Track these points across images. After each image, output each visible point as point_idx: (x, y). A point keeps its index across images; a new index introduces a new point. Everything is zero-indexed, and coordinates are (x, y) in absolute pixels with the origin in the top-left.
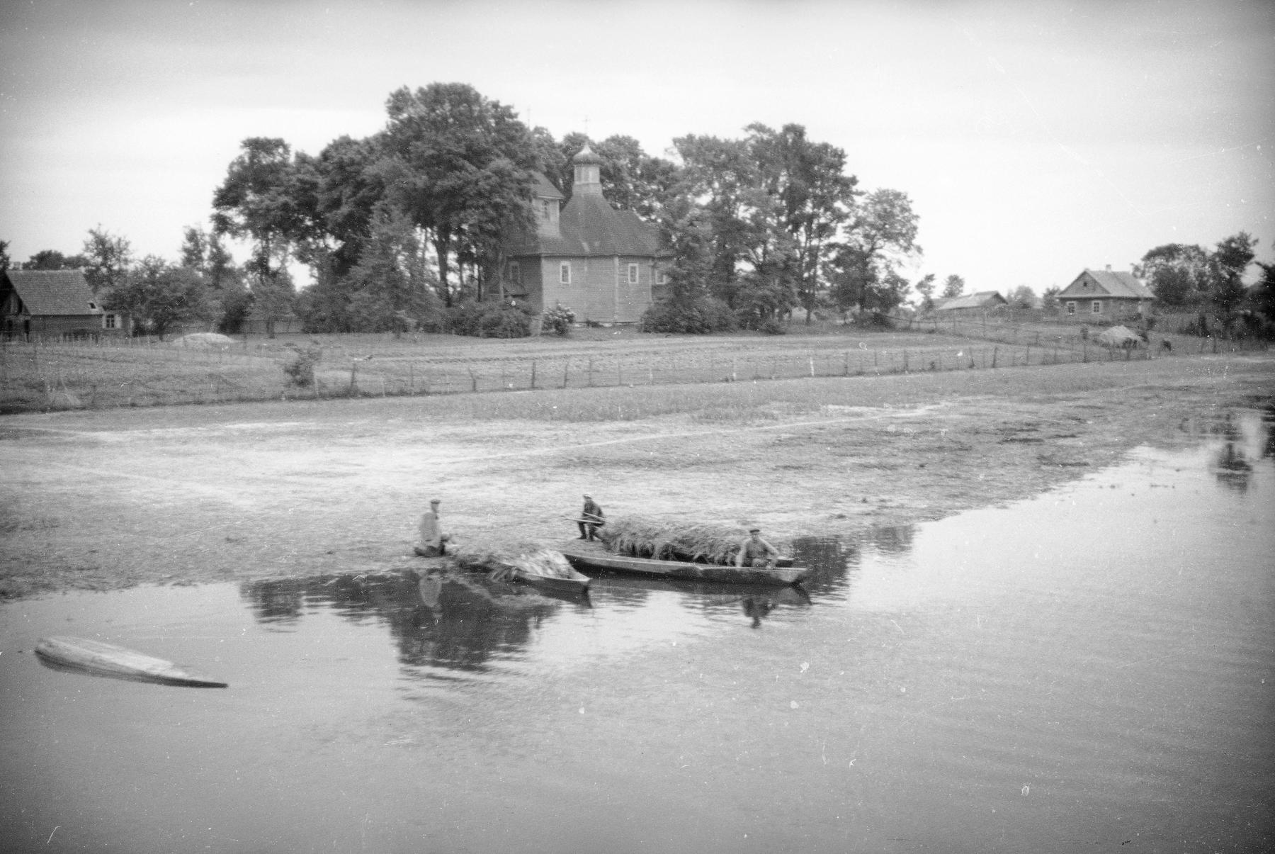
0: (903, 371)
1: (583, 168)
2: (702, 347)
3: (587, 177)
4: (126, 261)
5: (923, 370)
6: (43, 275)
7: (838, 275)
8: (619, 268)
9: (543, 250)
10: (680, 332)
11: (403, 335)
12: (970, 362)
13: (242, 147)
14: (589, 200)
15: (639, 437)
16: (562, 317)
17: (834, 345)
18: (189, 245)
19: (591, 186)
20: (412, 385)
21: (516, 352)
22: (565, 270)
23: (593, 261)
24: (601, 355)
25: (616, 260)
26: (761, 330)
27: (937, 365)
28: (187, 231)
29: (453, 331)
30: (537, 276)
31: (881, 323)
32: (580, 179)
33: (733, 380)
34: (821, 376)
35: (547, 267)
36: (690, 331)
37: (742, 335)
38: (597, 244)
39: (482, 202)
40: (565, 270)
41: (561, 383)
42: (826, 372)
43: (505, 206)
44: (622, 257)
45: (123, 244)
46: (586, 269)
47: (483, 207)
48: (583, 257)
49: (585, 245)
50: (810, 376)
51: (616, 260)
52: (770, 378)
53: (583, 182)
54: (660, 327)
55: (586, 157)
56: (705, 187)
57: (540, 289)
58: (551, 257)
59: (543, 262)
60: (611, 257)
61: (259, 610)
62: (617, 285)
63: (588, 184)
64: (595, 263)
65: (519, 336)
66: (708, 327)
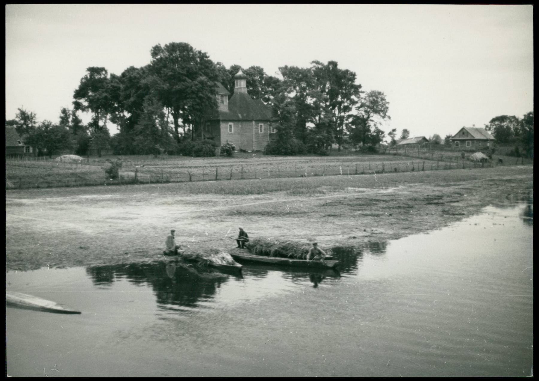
1: (239, 81)
3: (240, 85)
4: (35, 123)
9: (221, 118)
12: (412, 168)
13: (87, 71)
14: (242, 95)
19: (243, 89)
25: (254, 122)
27: (398, 170)
28: (62, 109)
32: (237, 85)
35: (223, 125)
37: (310, 156)
38: (245, 115)
40: (231, 126)
41: (229, 177)
43: (204, 98)
45: (33, 115)
46: (240, 126)
49: (240, 115)
50: (340, 174)
51: (254, 122)
53: (239, 87)
54: (273, 152)
59: (221, 123)
60: (252, 121)
64: (245, 124)
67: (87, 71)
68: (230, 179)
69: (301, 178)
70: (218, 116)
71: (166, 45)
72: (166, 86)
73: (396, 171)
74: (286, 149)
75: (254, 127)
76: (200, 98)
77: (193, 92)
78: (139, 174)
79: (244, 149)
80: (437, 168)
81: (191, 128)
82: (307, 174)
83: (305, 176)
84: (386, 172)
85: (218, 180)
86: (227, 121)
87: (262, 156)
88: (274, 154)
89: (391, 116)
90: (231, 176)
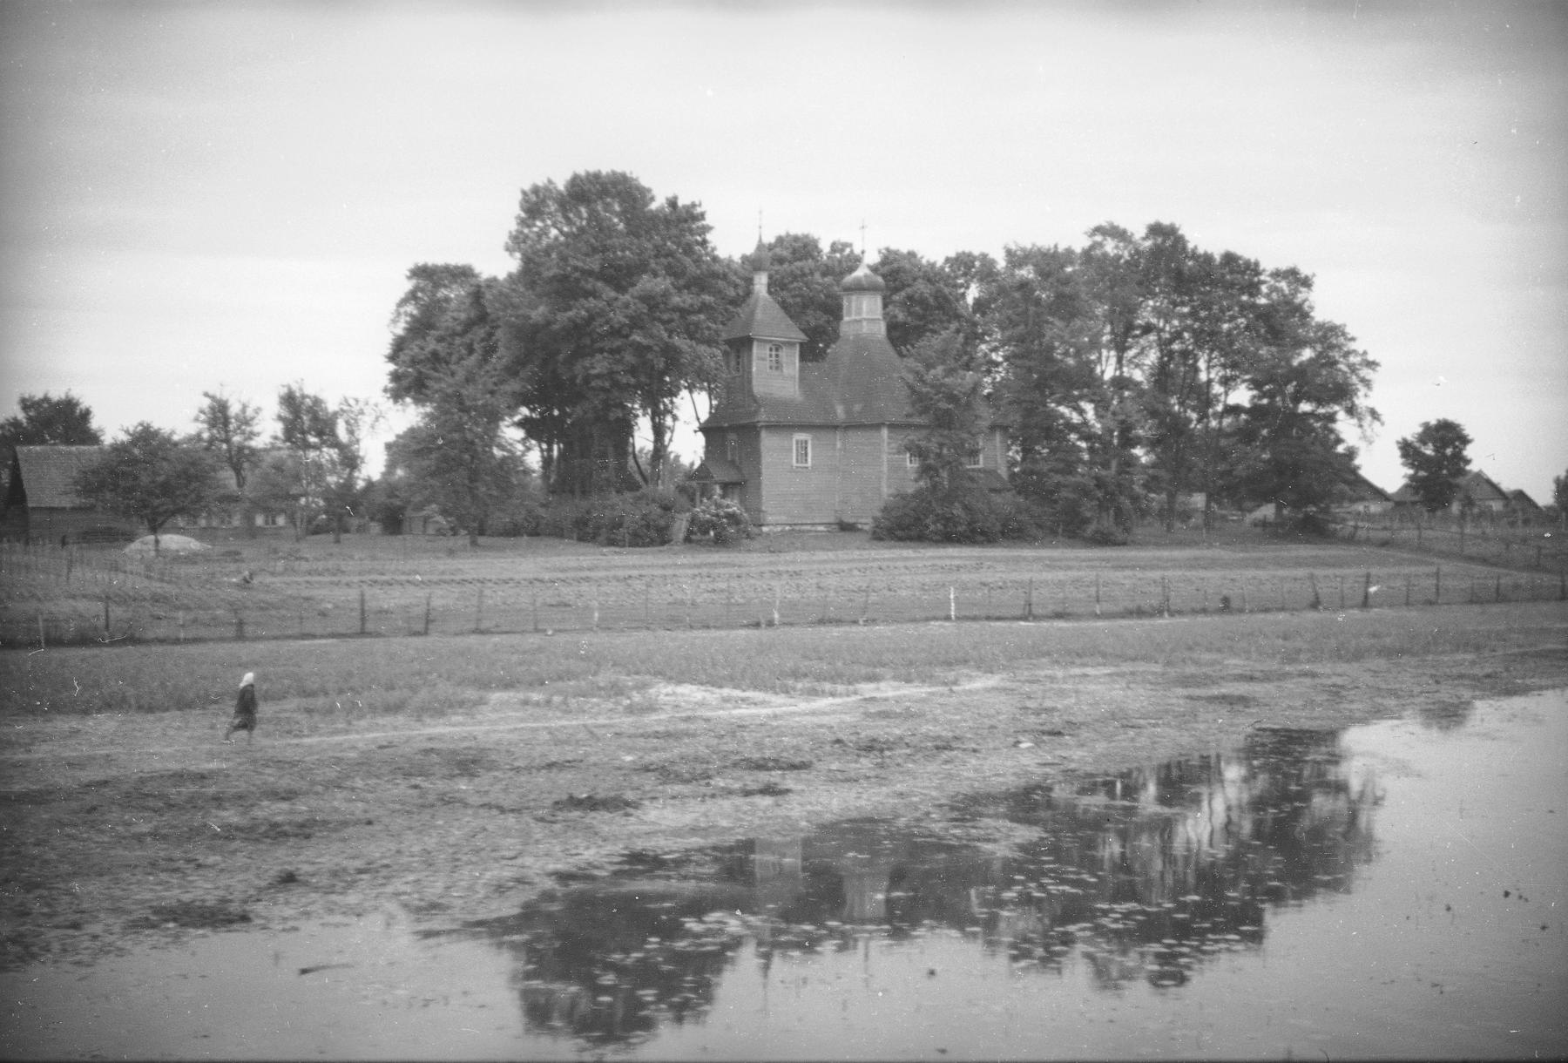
0: (1158, 612)
1: (854, 298)
2: (884, 564)
3: (859, 311)
4: (252, 435)
5: (1204, 611)
6: (70, 453)
7: (1428, 458)
8: (889, 444)
9: (762, 417)
10: (931, 540)
11: (344, 536)
12: (1312, 599)
13: (409, 278)
14: (861, 344)
15: (744, 711)
16: (717, 515)
17: (1213, 564)
18: (285, 413)
19: (865, 323)
20: (1206, 599)
21: (555, 569)
22: (803, 445)
23: (850, 433)
24: (906, 568)
25: (885, 432)
26: (1084, 539)
27: (1235, 604)
28: (284, 391)
29: (575, 536)
30: (755, 455)
31: (1314, 529)
32: (849, 314)
33: (770, 624)
34: (975, 619)
35: (768, 441)
36: (949, 537)
37: (1049, 546)
38: (857, 407)
39: (618, 343)
40: (803, 445)
41: (420, 627)
42: (983, 613)
43: (649, 348)
44: (893, 427)
45: (249, 412)
46: (839, 445)
47: (929, 366)
48: (836, 427)
49: (840, 410)
50: (948, 618)
51: (885, 432)
52: (855, 622)
53: (853, 317)
54: (899, 533)
55: (858, 280)
56: (538, 289)
57: (759, 474)
58: (774, 427)
59: (764, 434)
60: (877, 427)
61: (1195, 846)
62: (885, 468)
63: (860, 321)
64: (856, 437)
65: (652, 543)
66: (983, 533)
67: (409, 278)
68: (426, 633)
69: (1261, 616)
70: (756, 412)
71: (673, 203)
72: (539, 313)
73: (1226, 606)
74: (948, 520)
75: (885, 447)
76: (641, 350)
77: (616, 332)
78: (1502, 581)
79: (852, 521)
80: (1432, 597)
81: (555, 453)
82: (782, 615)
83: (770, 624)
84: (1036, 618)
85: (370, 635)
86: (781, 428)
87: (867, 545)
88: (901, 539)
89: (1379, 410)
90: (428, 621)
